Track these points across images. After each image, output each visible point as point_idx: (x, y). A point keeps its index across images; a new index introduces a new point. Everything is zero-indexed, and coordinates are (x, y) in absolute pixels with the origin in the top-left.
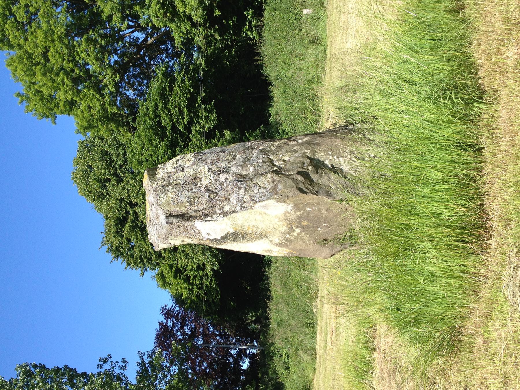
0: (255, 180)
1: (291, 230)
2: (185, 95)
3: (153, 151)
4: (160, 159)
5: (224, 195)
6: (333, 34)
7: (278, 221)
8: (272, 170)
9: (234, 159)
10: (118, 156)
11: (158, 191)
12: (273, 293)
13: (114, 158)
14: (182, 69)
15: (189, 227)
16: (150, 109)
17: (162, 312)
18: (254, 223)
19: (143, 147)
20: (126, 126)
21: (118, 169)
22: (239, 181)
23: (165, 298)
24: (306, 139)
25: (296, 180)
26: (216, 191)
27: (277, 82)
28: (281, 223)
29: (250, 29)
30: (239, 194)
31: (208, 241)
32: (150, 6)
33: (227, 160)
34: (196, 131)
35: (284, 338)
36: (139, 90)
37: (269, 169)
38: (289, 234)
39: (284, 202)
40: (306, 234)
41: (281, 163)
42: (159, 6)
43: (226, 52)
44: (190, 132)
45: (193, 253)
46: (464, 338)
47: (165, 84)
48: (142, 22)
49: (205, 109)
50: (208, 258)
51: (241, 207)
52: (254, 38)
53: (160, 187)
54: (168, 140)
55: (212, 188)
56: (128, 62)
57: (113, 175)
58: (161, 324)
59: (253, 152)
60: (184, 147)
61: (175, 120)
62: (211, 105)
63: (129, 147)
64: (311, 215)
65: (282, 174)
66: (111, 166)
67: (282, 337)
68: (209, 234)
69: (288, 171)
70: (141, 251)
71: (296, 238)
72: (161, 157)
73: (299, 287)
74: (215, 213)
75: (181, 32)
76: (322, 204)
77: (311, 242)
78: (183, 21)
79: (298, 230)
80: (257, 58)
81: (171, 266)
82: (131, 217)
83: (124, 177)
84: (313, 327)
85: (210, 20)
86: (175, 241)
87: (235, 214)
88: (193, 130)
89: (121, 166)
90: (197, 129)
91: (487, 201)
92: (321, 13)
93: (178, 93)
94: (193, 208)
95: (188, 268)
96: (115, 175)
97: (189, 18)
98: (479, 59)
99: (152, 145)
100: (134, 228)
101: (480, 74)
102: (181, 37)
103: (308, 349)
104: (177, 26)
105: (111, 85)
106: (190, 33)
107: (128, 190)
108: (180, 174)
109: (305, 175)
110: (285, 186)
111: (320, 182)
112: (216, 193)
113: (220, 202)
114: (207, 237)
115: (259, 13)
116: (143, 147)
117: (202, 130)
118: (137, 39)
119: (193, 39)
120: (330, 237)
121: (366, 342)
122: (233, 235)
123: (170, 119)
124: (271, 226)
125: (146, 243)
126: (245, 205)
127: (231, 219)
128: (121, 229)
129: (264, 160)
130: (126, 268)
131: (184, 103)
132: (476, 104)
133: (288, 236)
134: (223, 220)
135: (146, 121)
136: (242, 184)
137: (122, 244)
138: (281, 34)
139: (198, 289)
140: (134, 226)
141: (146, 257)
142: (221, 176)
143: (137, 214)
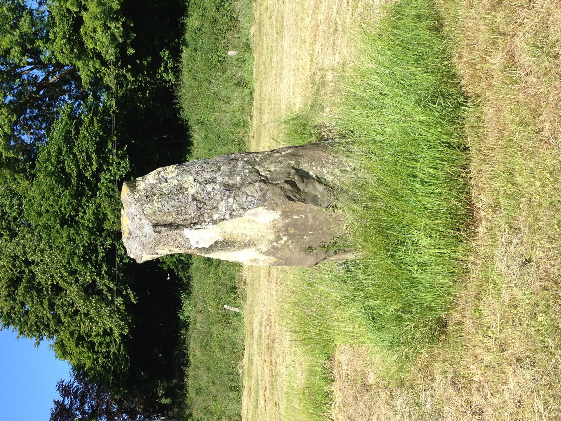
0: (243, 189)
1: (279, 238)
2: (94, 139)
3: (54, 200)
4: (63, 210)
5: (212, 204)
6: (264, 76)
7: (266, 229)
8: (259, 179)
9: (220, 170)
10: (12, 207)
11: (142, 201)
12: (191, 358)
13: (7, 210)
14: (90, 110)
15: (178, 236)
16: (52, 154)
17: (58, 389)
18: (243, 231)
19: (43, 197)
20: (23, 173)
21: (12, 223)
22: (227, 190)
23: (64, 371)
24: (289, 151)
25: (284, 188)
26: (203, 200)
27: (198, 126)
28: (270, 231)
29: (166, 70)
30: (228, 202)
31: (196, 250)
32: (54, 41)
33: (212, 171)
34: (105, 179)
35: (204, 407)
36: (37, 134)
37: (256, 178)
38: (277, 241)
39: (274, 209)
40: (293, 242)
41: (267, 173)
42: (65, 40)
43: (140, 94)
44: (98, 180)
45: (98, 316)
46: (450, 328)
47: (70, 126)
48: (45, 56)
49: (117, 155)
50: (116, 322)
51: (231, 215)
52: (170, 80)
53: (144, 198)
54: (73, 189)
55: (199, 197)
56: (27, 101)
57: (5, 229)
58: (57, 402)
59: (239, 163)
60: (92, 197)
61: (81, 166)
62: (123, 150)
63: (25, 197)
64: (298, 223)
65: (269, 183)
66: (4, 219)
67: (202, 407)
68: (197, 242)
69: (275, 180)
70: (37, 317)
71: (283, 246)
72: (65, 208)
73: (222, 348)
74: (204, 221)
75: (89, 70)
76: (309, 212)
77: (297, 250)
78: (92, 58)
79: (285, 239)
80: (175, 101)
81: (72, 333)
82: (26, 277)
83: (19, 231)
84: (238, 391)
85: (123, 59)
86: (162, 251)
87: (225, 222)
88: (102, 178)
89: (15, 219)
90: (107, 177)
91: (474, 193)
92: (247, 56)
93: (85, 137)
94: (181, 217)
95: (93, 334)
96: (8, 228)
97: (99, 56)
98: (461, 68)
99: (54, 194)
100: (29, 289)
101: (463, 83)
102: (88, 76)
103: (233, 416)
104: (84, 64)
105: (6, 126)
106: (99, 72)
107: (24, 246)
108: (163, 185)
109: (292, 184)
110: (274, 194)
111: (306, 191)
112: (203, 202)
113: (209, 211)
114: (195, 246)
115: (176, 54)
116: (43, 197)
117: (112, 178)
118: (37, 77)
119: (102, 79)
120: (314, 245)
121: (324, 374)
122: (222, 243)
123: (75, 165)
124: (260, 234)
125: (43, 307)
126: (234, 213)
127: (221, 227)
128: (14, 291)
129: (251, 170)
130: (18, 337)
131: (92, 147)
132: (462, 108)
133: (275, 244)
134: (213, 228)
135: (47, 167)
136: (230, 192)
137: (14, 309)
138: (203, 76)
139: (104, 358)
140: (29, 288)
141: (43, 323)
142: (207, 186)
143: (33, 273)
